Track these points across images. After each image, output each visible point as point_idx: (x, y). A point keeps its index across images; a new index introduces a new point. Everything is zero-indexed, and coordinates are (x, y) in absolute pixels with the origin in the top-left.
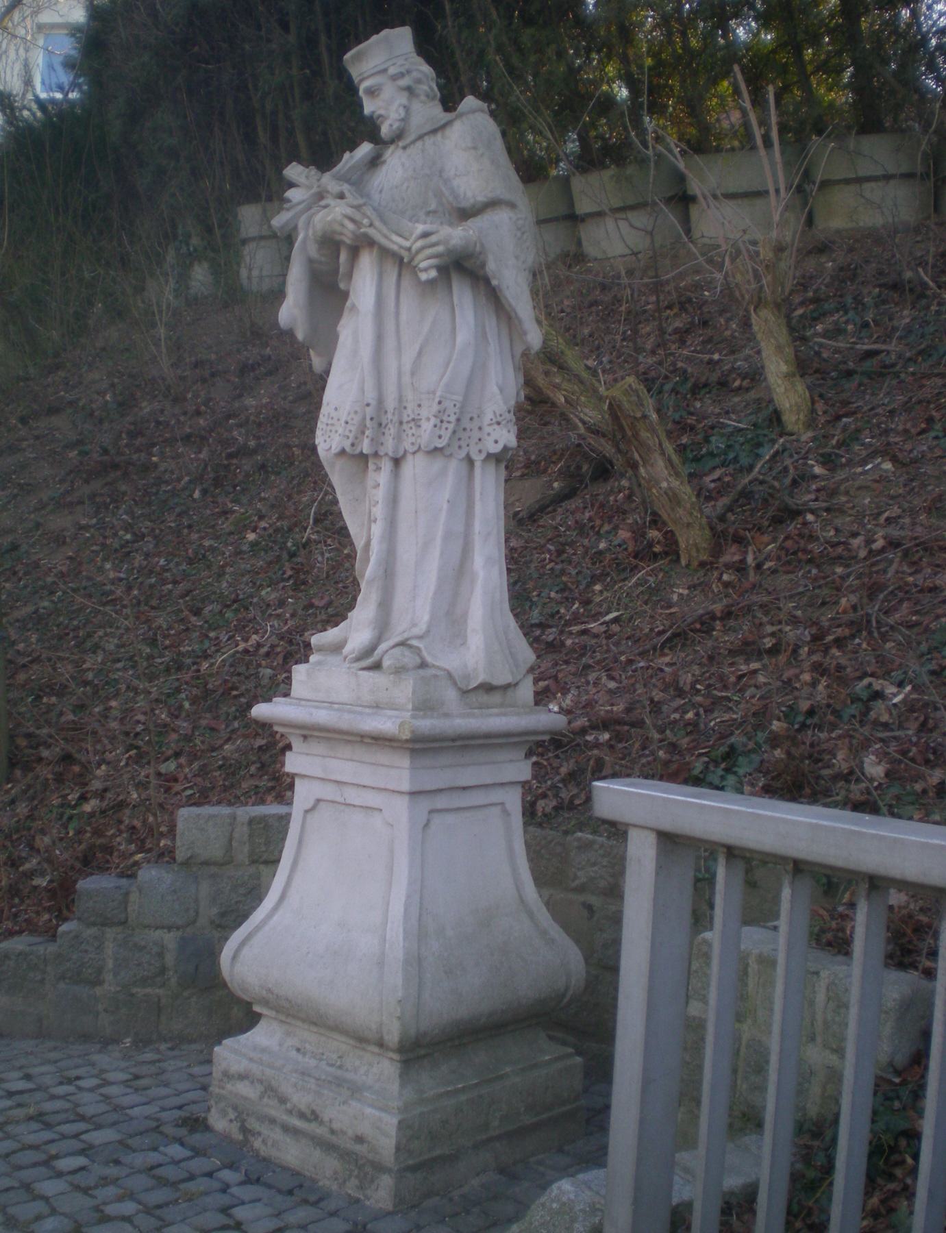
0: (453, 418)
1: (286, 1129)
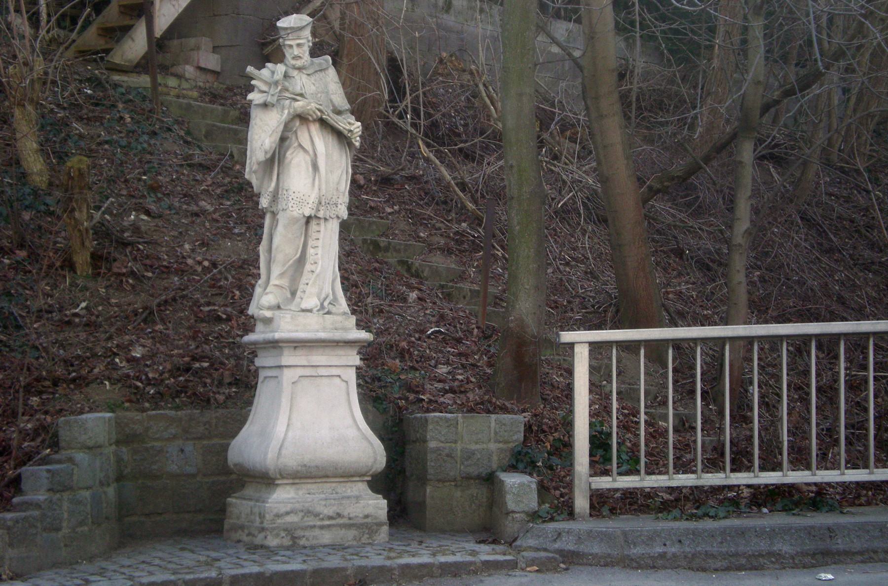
1: (322, 527)
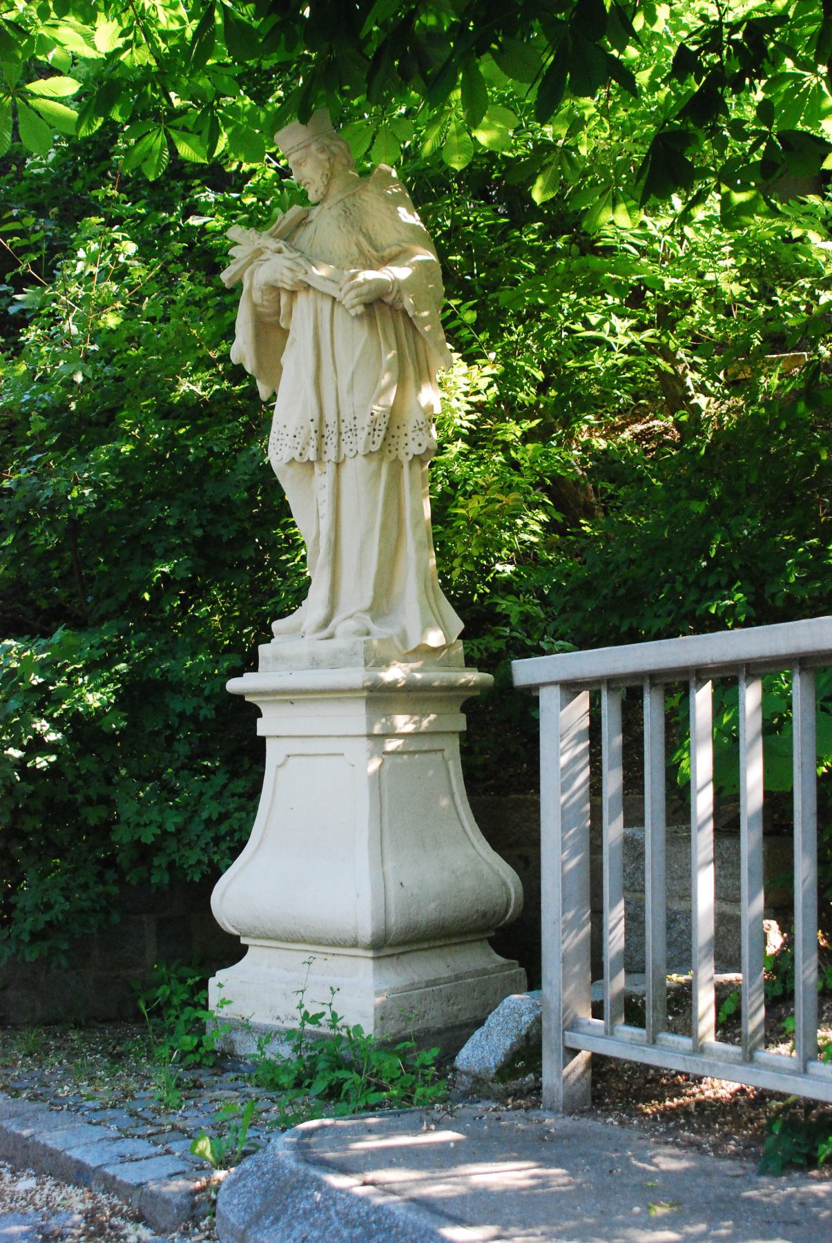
0: (383, 427)
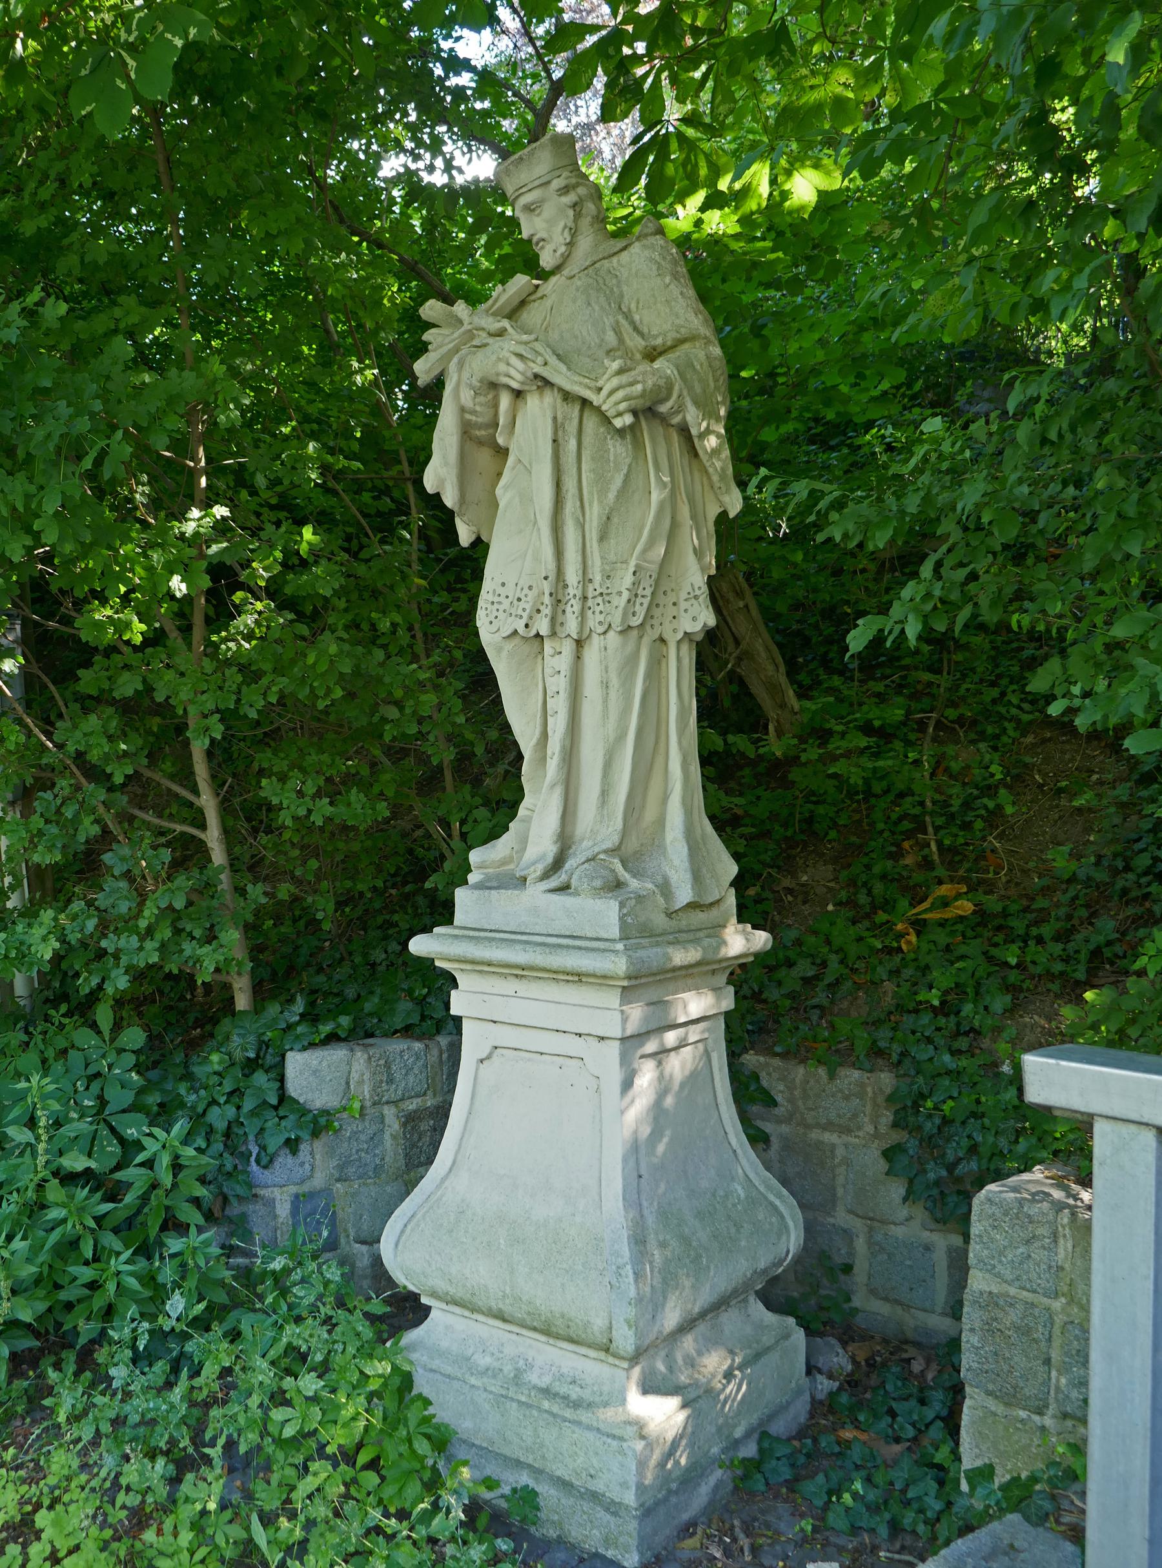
0: (648, 592)
